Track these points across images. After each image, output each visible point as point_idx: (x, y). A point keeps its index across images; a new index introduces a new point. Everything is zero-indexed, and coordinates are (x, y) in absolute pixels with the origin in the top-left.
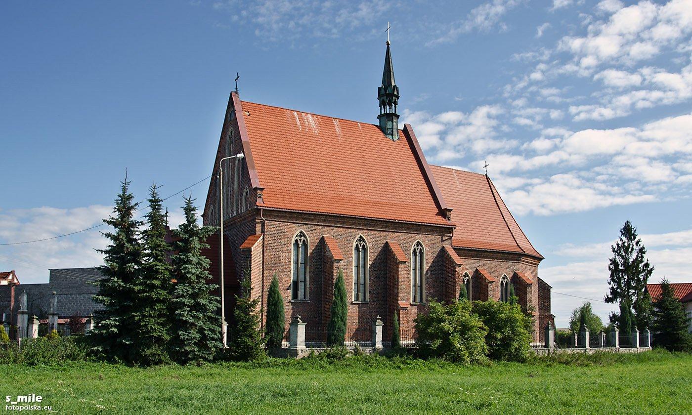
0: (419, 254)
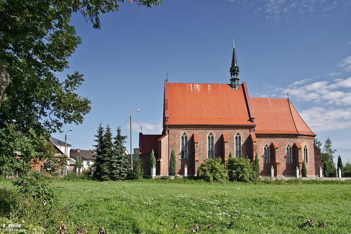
0: (238, 139)
